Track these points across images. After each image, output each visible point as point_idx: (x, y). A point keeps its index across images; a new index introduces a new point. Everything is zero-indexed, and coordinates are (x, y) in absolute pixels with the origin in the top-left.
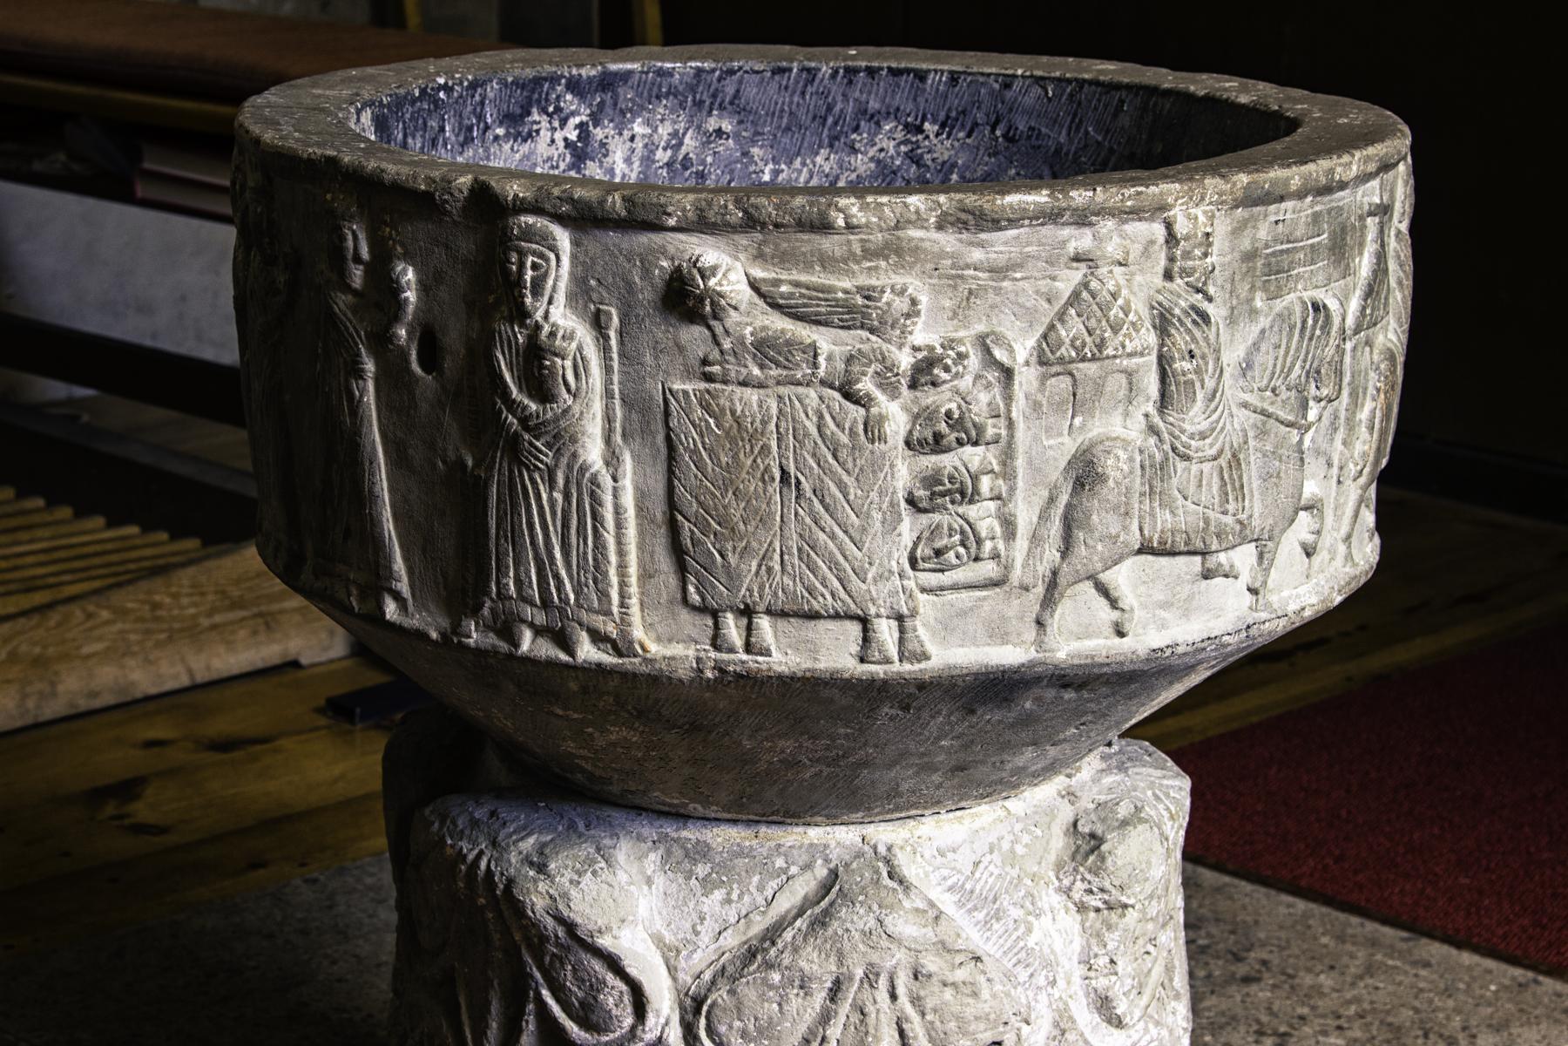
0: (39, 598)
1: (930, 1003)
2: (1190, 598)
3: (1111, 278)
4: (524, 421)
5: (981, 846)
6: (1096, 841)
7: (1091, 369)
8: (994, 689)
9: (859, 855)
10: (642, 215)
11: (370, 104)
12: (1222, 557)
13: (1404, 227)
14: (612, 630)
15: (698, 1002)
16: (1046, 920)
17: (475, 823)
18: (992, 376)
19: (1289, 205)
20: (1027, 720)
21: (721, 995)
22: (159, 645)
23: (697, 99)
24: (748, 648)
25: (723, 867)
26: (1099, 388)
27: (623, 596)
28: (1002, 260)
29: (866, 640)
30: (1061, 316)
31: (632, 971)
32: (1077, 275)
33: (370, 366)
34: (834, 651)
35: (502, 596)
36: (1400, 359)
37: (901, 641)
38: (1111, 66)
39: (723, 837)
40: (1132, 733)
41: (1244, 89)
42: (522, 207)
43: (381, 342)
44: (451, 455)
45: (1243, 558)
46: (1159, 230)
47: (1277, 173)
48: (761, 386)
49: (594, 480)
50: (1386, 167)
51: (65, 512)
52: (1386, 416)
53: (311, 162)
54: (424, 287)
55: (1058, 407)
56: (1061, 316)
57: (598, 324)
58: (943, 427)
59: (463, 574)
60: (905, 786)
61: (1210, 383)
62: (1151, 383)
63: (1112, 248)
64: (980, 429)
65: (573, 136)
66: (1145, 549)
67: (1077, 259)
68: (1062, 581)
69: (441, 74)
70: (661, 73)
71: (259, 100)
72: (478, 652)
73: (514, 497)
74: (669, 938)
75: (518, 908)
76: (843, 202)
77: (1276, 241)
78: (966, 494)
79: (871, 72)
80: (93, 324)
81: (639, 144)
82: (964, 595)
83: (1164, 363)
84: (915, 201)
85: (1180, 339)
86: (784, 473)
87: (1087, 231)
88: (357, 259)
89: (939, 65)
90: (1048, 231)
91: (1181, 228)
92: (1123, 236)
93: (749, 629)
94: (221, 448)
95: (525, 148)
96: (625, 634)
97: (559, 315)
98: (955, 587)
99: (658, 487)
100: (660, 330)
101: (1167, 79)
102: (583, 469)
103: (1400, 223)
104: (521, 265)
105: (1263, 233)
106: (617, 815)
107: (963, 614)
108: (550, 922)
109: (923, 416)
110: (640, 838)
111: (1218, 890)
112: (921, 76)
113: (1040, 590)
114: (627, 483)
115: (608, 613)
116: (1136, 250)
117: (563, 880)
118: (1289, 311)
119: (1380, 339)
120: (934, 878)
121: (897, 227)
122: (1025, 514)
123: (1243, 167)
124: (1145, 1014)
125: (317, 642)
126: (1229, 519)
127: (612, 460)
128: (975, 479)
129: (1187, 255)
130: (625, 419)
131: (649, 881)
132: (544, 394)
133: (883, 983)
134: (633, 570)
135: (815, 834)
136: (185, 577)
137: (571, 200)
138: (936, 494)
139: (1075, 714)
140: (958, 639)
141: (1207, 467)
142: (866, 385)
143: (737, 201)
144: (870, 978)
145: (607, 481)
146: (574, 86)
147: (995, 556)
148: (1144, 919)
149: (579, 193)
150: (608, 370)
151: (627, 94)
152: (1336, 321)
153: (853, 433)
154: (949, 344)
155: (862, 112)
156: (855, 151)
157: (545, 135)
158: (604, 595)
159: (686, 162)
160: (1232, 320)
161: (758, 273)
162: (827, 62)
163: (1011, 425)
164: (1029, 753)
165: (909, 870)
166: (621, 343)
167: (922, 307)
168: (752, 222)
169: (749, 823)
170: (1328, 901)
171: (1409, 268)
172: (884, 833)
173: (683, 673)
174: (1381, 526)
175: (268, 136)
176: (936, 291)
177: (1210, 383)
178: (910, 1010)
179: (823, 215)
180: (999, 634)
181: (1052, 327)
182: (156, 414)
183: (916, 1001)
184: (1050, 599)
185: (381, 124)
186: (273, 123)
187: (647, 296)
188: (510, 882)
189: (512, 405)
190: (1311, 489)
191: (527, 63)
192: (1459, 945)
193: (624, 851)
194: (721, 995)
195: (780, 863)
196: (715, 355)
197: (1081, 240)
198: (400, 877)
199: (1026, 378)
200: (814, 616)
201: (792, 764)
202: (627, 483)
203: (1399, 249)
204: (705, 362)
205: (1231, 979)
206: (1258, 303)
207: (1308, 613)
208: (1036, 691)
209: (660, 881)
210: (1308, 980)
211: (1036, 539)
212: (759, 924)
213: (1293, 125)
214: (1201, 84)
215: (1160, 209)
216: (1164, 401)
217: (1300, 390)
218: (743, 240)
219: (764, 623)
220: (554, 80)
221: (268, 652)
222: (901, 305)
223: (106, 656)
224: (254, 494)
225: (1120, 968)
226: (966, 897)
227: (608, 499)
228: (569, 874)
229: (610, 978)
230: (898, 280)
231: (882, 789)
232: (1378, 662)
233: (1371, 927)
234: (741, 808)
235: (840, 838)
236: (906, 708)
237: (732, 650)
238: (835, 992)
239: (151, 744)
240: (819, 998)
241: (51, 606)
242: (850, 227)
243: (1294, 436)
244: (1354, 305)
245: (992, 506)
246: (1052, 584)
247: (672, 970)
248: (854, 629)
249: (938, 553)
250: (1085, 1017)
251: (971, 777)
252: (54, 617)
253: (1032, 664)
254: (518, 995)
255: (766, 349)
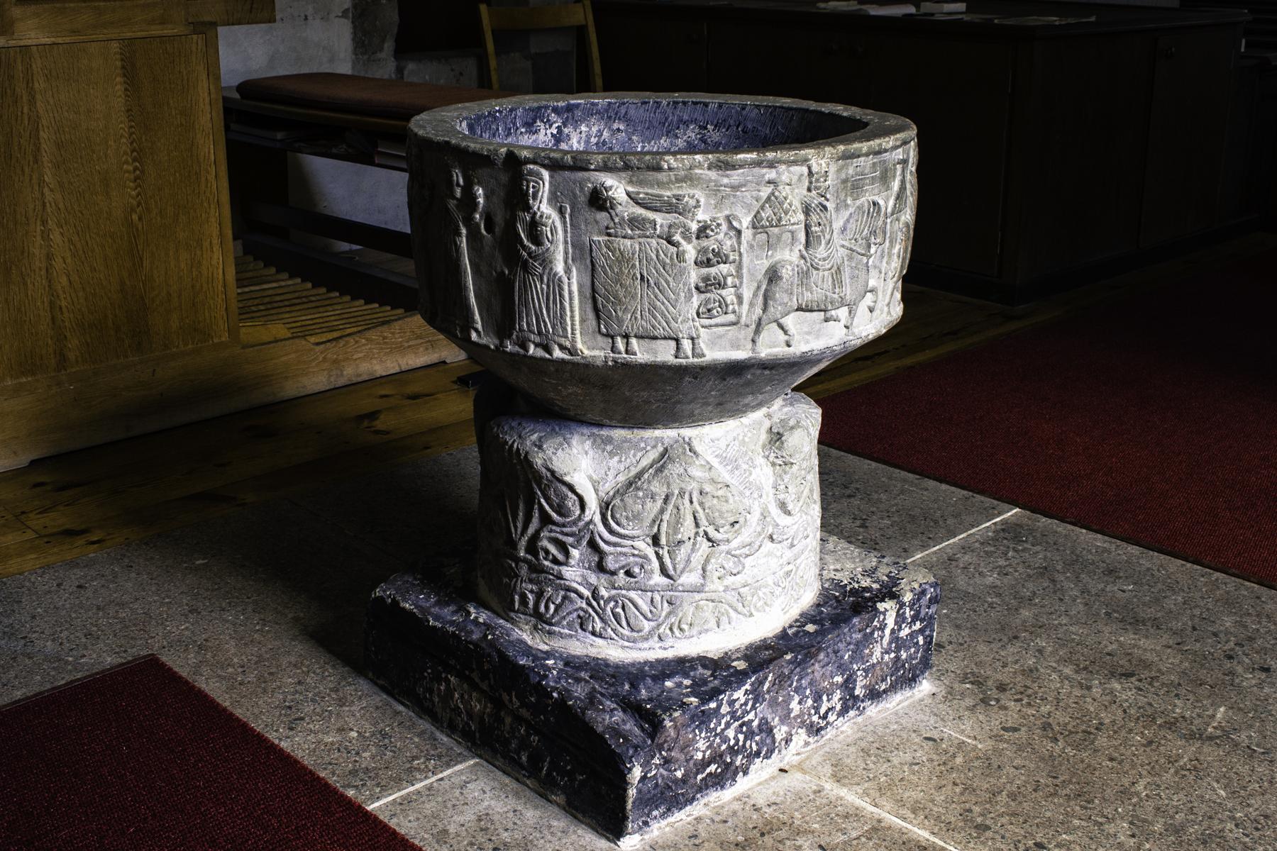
0: (335, 334)
1: (707, 505)
2: (819, 330)
3: (785, 191)
4: (529, 254)
5: (730, 438)
6: (780, 435)
7: (776, 230)
8: (734, 369)
9: (677, 441)
10: (579, 164)
11: (466, 118)
12: (833, 313)
13: (914, 169)
14: (568, 344)
15: (608, 504)
16: (758, 469)
17: (512, 428)
18: (732, 233)
19: (862, 159)
20: (749, 383)
21: (617, 501)
22: (386, 354)
23: (608, 115)
24: (627, 352)
25: (619, 447)
26: (779, 238)
27: (573, 329)
28: (736, 183)
29: (678, 348)
30: (762, 207)
31: (579, 491)
32: (769, 189)
33: (464, 231)
34: (664, 353)
35: (521, 330)
36: (912, 227)
37: (693, 349)
38: (788, 100)
39: (618, 434)
40: (795, 389)
41: (845, 110)
42: (528, 161)
43: (469, 221)
44: (499, 269)
45: (843, 313)
46: (805, 170)
47: (856, 145)
48: (632, 238)
49: (560, 280)
50: (905, 143)
51: (348, 298)
52: (905, 251)
53: (438, 143)
54: (487, 197)
55: (761, 247)
56: (762, 207)
57: (561, 212)
58: (711, 256)
59: (504, 322)
60: (696, 412)
61: (827, 237)
62: (802, 237)
63: (785, 178)
64: (727, 256)
65: (555, 132)
66: (799, 309)
67: (769, 182)
68: (763, 323)
69: (497, 105)
70: (593, 104)
71: (418, 117)
72: (511, 354)
73: (525, 287)
74: (595, 477)
75: (530, 464)
76: (667, 158)
77: (857, 174)
78: (721, 285)
79: (684, 103)
80: (360, 218)
81: (583, 135)
82: (720, 329)
83: (807, 227)
84: (698, 157)
85: (814, 218)
86: (642, 276)
87: (774, 170)
88: (458, 185)
89: (714, 100)
90: (757, 170)
91: (815, 169)
92: (789, 172)
93: (627, 343)
94: (404, 269)
95: (534, 137)
96: (574, 346)
97: (545, 208)
98: (717, 325)
99: (589, 283)
100: (589, 214)
101: (812, 105)
102: (555, 274)
103: (912, 167)
104: (528, 186)
105: (851, 171)
106: (573, 425)
107: (720, 337)
108: (544, 470)
109: (703, 251)
110: (583, 434)
111: (838, 458)
112: (706, 105)
113: (754, 326)
114: (574, 280)
115: (566, 337)
116: (795, 179)
117: (549, 452)
118: (862, 205)
119: (903, 218)
120: (710, 452)
121: (690, 168)
122: (747, 294)
123: (842, 142)
124: (800, 510)
125: (453, 354)
126: (836, 296)
127: (568, 271)
128: (725, 278)
129: (817, 181)
130: (574, 253)
131: (586, 453)
132: (538, 242)
133: (687, 496)
134: (577, 318)
135: (658, 433)
136: (397, 325)
137: (549, 158)
138: (707, 285)
139: (770, 381)
140: (716, 351)
141: (826, 273)
142: (677, 238)
143: (621, 158)
144: (682, 494)
145: (565, 280)
146: (555, 110)
147: (734, 312)
148: (800, 469)
149: (552, 155)
150: (566, 231)
151: (578, 113)
152: (883, 210)
153: (671, 259)
154: (713, 220)
155: (681, 120)
156: (677, 138)
157: (543, 131)
158: (565, 329)
159: (604, 143)
160: (837, 209)
161: (630, 189)
162: (665, 99)
163: (740, 255)
164: (750, 398)
165: (698, 448)
166: (571, 220)
167: (701, 204)
168: (627, 167)
169: (629, 428)
170: (885, 463)
171: (916, 187)
172: (687, 432)
173: (599, 363)
174: (903, 299)
175: (421, 132)
176: (708, 196)
177: (827, 237)
178: (698, 508)
179: (658, 164)
180: (736, 346)
181: (758, 212)
182: (390, 256)
183: (701, 504)
184: (758, 331)
185: (471, 127)
186: (423, 127)
187: (582, 199)
188: (527, 453)
189: (524, 247)
190: (872, 283)
191: (535, 100)
192: (941, 482)
193: (575, 440)
194: (617, 501)
195: (643, 445)
196: (612, 225)
197: (771, 174)
198: (481, 452)
199: (747, 234)
200: (655, 338)
201: (647, 402)
202: (574, 280)
203: (911, 179)
204: (607, 228)
205: (843, 496)
206: (849, 202)
207: (871, 337)
208: (752, 371)
209: (591, 452)
210: (876, 496)
211: (751, 305)
212: (634, 471)
213: (866, 124)
214: (827, 108)
215: (805, 161)
216: (808, 244)
217: (867, 239)
218: (623, 175)
219: (634, 341)
220: (546, 107)
221: (432, 357)
222: (692, 202)
223: (364, 358)
224: (417, 286)
225: (790, 490)
226: (724, 460)
227: (566, 288)
228: (552, 450)
229: (570, 494)
230: (691, 192)
231: (687, 413)
232: (908, 361)
233: (904, 474)
234: (626, 421)
235: (668, 434)
236: (696, 378)
237: (620, 353)
238: (666, 500)
239: (382, 396)
240: (659, 503)
241: (341, 337)
242: (670, 169)
243: (865, 260)
244: (891, 203)
245: (732, 290)
246: (759, 324)
247: (596, 491)
248: (673, 343)
249: (709, 310)
250: (775, 511)
251: (725, 408)
252: (342, 343)
253: (750, 359)
254: (531, 501)
255: (634, 222)
